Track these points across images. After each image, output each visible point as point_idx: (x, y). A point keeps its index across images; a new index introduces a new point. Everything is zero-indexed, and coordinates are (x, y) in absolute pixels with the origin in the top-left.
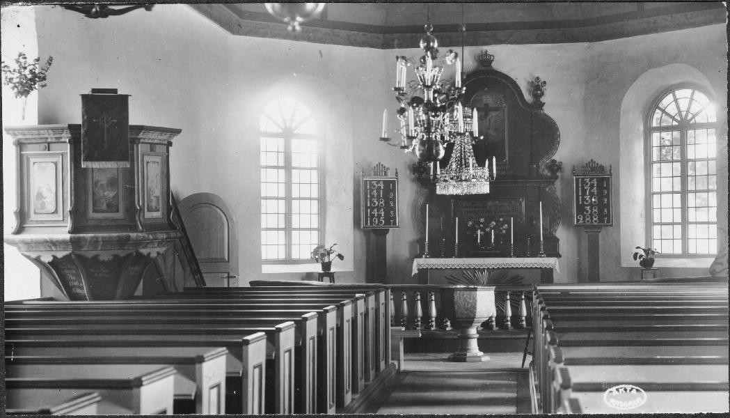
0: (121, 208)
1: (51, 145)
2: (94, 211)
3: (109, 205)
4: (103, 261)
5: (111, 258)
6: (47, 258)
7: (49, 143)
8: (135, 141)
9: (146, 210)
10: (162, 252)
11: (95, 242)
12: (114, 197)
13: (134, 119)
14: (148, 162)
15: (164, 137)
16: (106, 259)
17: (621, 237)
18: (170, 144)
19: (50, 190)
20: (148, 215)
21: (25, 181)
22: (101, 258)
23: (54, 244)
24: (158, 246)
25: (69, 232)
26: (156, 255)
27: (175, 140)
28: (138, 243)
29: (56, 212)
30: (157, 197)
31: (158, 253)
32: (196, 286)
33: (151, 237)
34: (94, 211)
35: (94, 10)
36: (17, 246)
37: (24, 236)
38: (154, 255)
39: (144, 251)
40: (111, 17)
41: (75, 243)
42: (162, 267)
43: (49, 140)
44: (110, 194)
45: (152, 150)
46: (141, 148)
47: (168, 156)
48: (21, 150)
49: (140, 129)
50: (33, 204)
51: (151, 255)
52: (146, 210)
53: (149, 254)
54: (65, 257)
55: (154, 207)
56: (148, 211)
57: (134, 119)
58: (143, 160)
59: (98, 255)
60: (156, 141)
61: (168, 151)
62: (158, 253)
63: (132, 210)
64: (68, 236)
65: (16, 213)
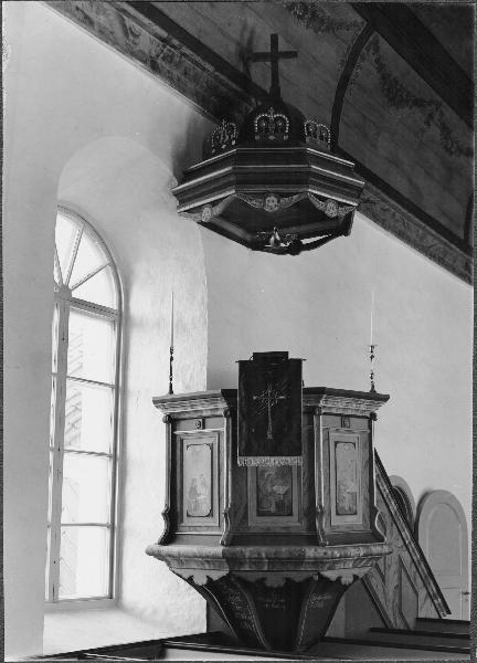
0: (360, 512)
1: (207, 420)
2: (260, 514)
3: (280, 505)
4: (271, 588)
5: (282, 583)
6: (201, 580)
7: (204, 418)
8: (312, 412)
9: (333, 513)
10: (361, 576)
11: (257, 561)
12: (286, 493)
13: (309, 380)
14: (336, 443)
15: (363, 407)
16: (275, 586)
17: (205, 344)
18: (373, 417)
19: (204, 484)
20: (337, 521)
21: (178, 470)
22: (268, 584)
23: (209, 560)
24: (354, 567)
25: (222, 544)
26: (351, 580)
27: (382, 411)
28: (318, 562)
29: (211, 514)
30: (354, 496)
31: (356, 577)
32: (437, 617)
33: (337, 554)
34: (260, 514)
35: (272, 238)
36: (166, 561)
37: (173, 549)
38: (347, 579)
39: (331, 575)
40: (304, 253)
41: (230, 559)
42: (381, 596)
43: (204, 414)
44: (280, 489)
45: (343, 425)
46: (322, 422)
47: (370, 435)
48: (174, 429)
49: (319, 392)
50: (188, 504)
51: (343, 580)
52: (333, 513)
53: (339, 579)
54: (223, 578)
55: (347, 508)
56: (337, 514)
57: (309, 380)
58: (327, 439)
59: (264, 579)
60: (349, 413)
61: (370, 427)
62: (356, 577)
63: (312, 513)
64: (219, 550)
65: (164, 514)
